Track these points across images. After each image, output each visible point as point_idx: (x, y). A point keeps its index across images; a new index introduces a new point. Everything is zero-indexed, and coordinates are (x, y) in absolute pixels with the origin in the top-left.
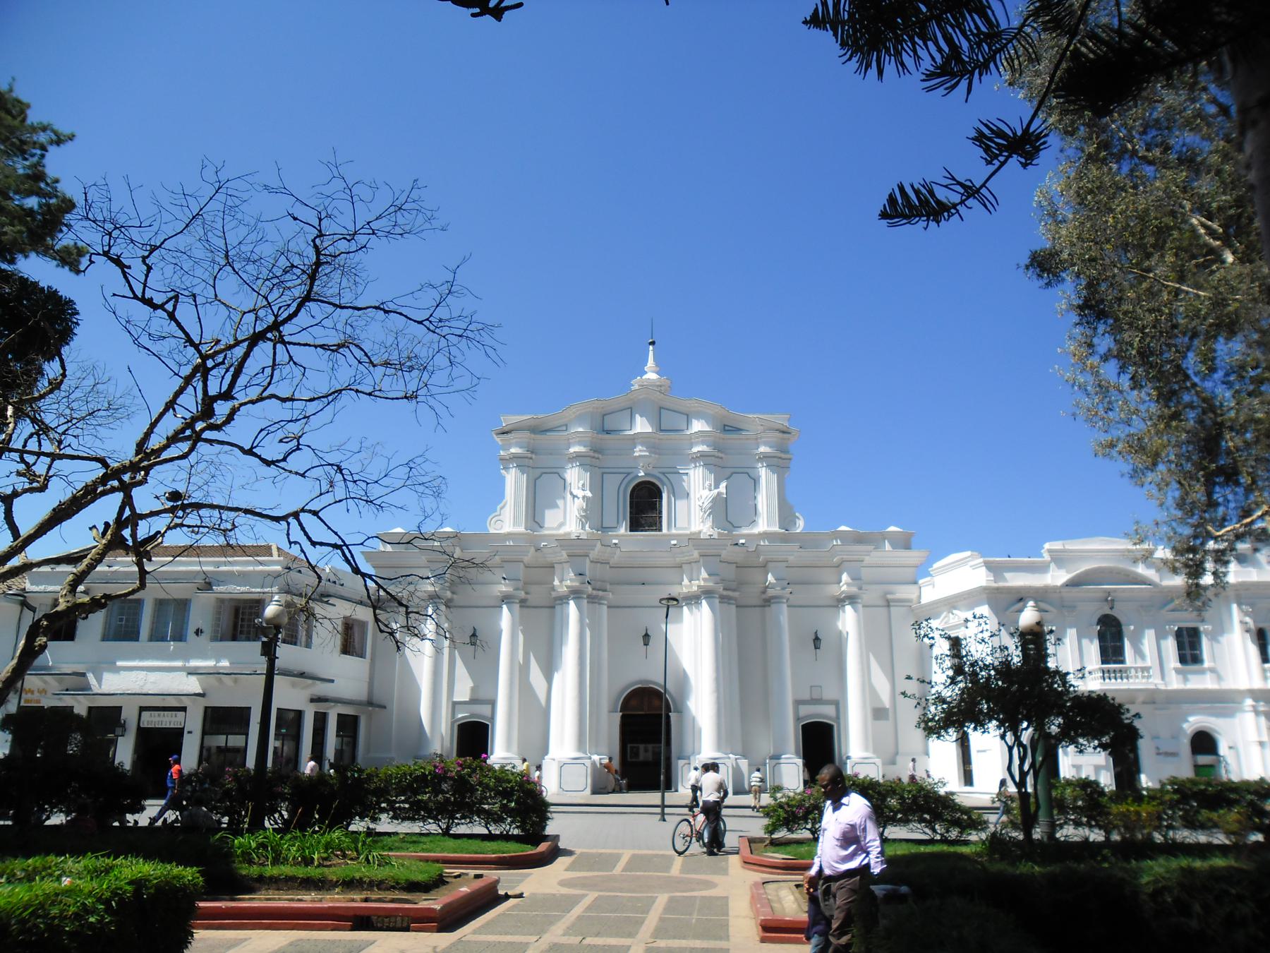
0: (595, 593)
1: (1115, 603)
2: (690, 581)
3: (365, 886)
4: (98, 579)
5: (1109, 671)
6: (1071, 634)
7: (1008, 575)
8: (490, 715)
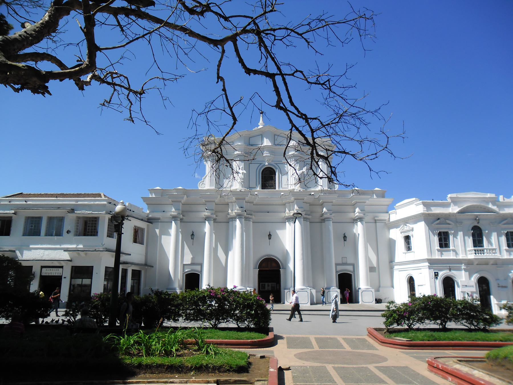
0: (247, 216)
1: (480, 221)
2: (289, 211)
3: (210, 370)
4: (20, 208)
5: (478, 251)
6: (461, 234)
7: (432, 208)
8: (200, 270)
